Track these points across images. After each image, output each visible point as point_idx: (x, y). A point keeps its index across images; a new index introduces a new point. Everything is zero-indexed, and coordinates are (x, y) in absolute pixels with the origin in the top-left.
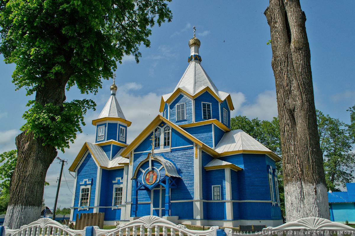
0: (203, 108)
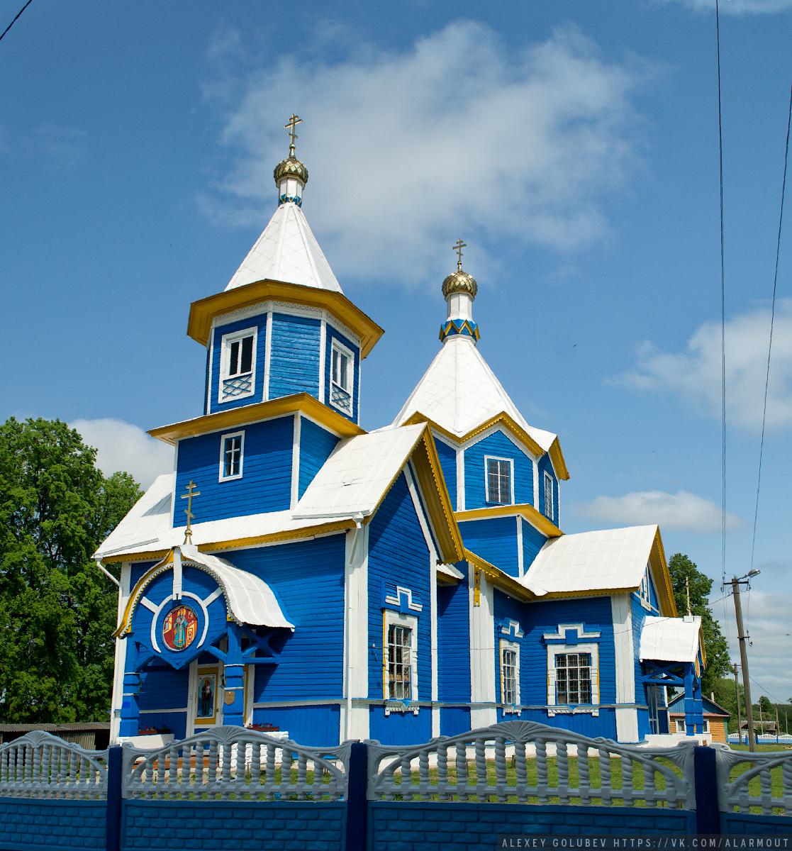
0: (490, 471)
